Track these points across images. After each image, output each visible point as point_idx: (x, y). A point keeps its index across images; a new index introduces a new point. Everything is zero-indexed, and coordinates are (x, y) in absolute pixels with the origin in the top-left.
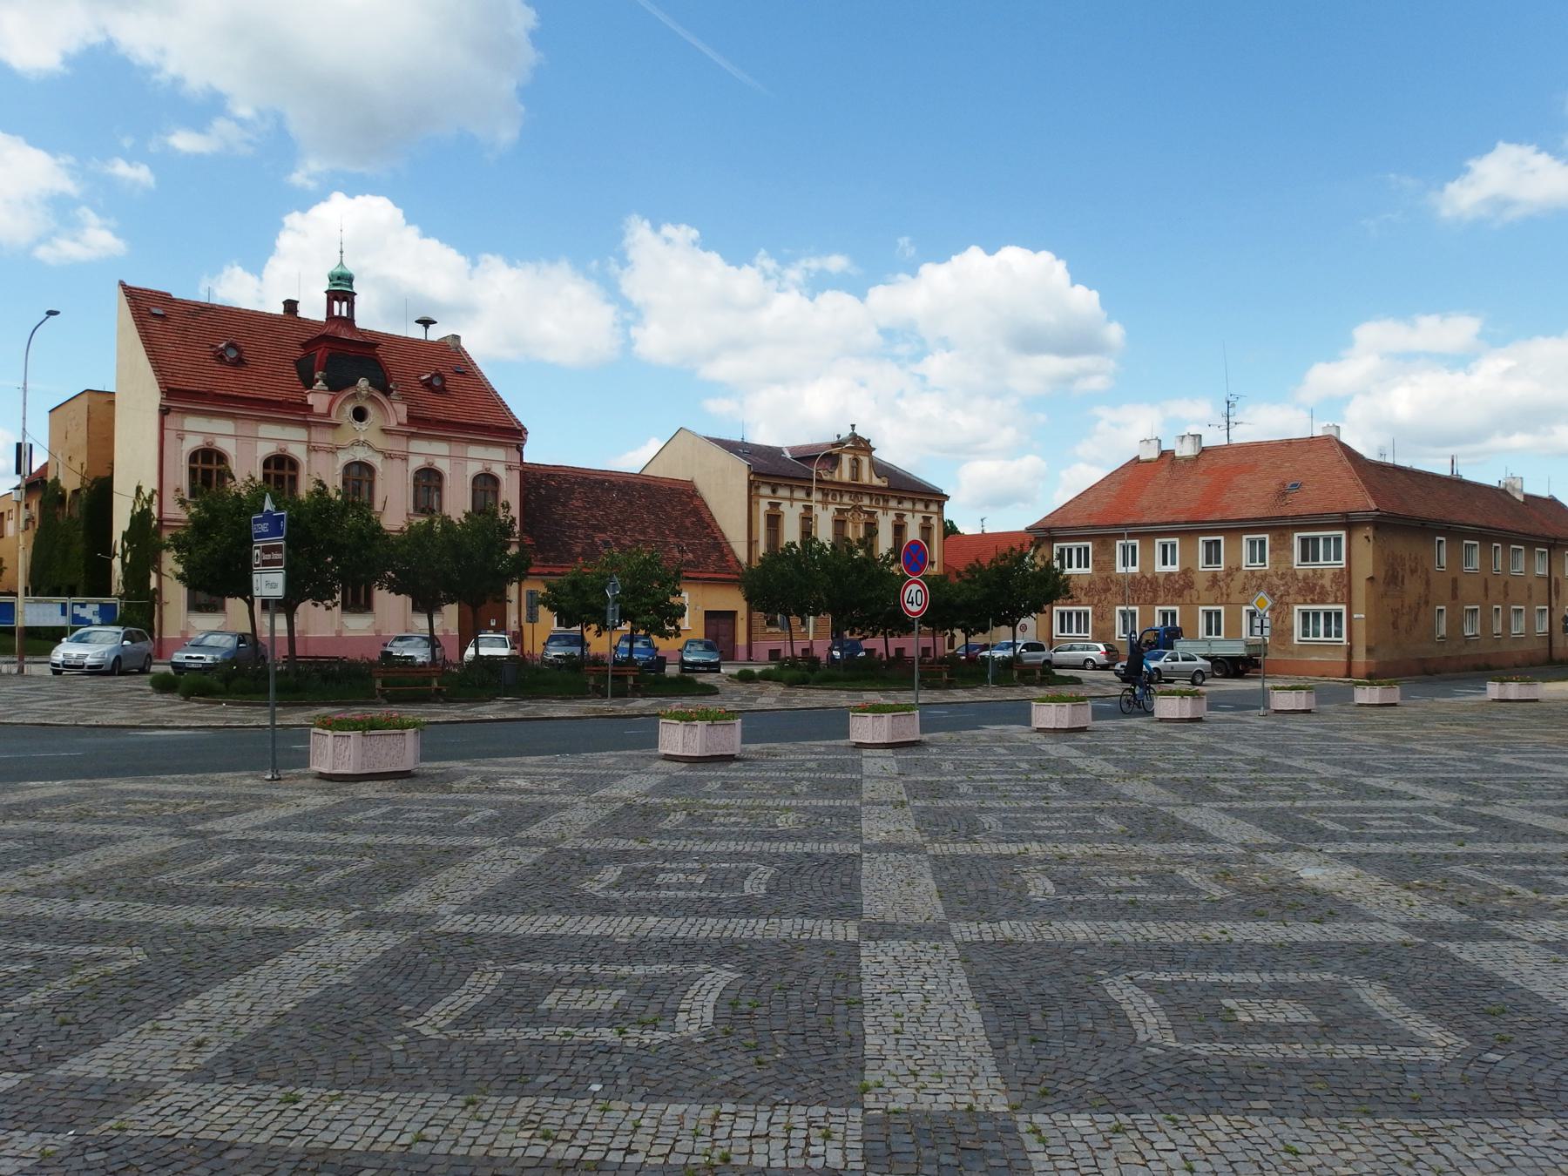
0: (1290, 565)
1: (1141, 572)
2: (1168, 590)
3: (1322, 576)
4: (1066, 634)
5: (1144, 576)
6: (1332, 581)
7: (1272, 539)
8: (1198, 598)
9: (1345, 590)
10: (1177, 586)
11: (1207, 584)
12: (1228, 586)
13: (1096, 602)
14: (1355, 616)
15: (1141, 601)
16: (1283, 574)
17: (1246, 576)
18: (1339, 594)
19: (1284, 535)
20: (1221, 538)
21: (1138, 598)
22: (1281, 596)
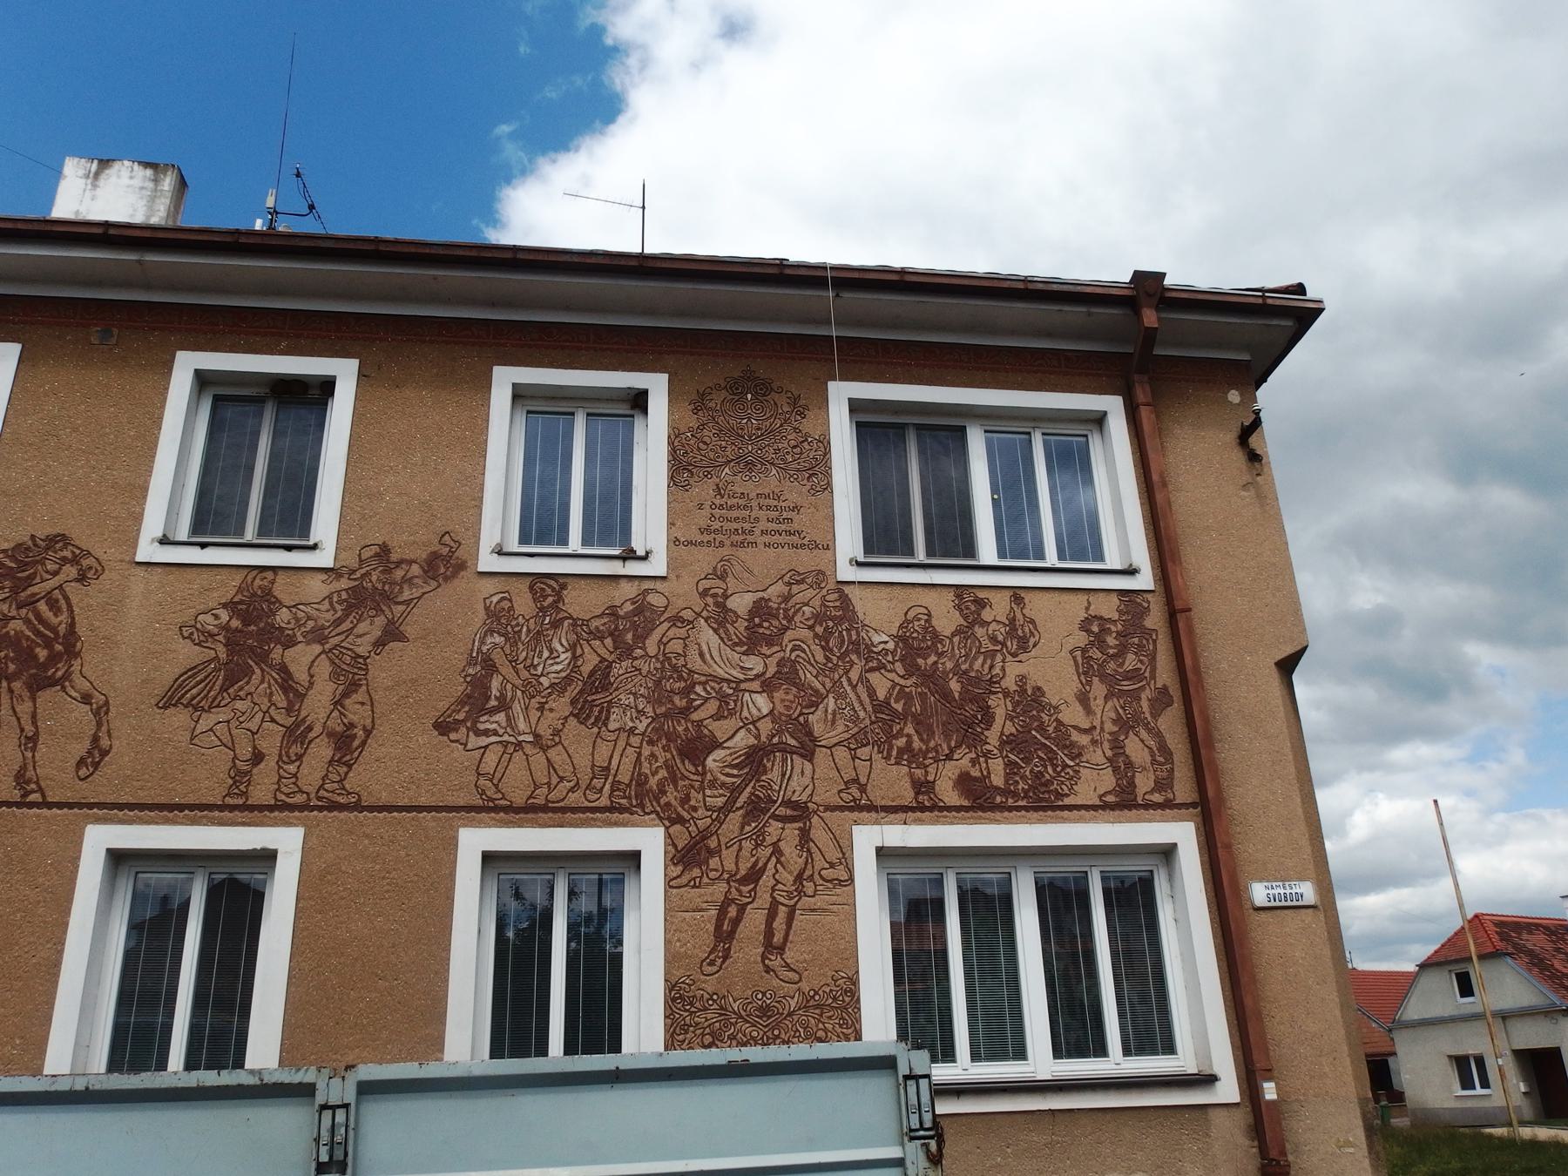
0: (806, 561)
3: (1020, 637)
6: (1087, 668)
8: (95, 756)
9: (1170, 723)
11: (188, 654)
12: (351, 677)
14: (1260, 893)
16: (760, 609)
17: (498, 617)
18: (1136, 749)
19: (763, 389)
20: (345, 372)
22: (755, 759)
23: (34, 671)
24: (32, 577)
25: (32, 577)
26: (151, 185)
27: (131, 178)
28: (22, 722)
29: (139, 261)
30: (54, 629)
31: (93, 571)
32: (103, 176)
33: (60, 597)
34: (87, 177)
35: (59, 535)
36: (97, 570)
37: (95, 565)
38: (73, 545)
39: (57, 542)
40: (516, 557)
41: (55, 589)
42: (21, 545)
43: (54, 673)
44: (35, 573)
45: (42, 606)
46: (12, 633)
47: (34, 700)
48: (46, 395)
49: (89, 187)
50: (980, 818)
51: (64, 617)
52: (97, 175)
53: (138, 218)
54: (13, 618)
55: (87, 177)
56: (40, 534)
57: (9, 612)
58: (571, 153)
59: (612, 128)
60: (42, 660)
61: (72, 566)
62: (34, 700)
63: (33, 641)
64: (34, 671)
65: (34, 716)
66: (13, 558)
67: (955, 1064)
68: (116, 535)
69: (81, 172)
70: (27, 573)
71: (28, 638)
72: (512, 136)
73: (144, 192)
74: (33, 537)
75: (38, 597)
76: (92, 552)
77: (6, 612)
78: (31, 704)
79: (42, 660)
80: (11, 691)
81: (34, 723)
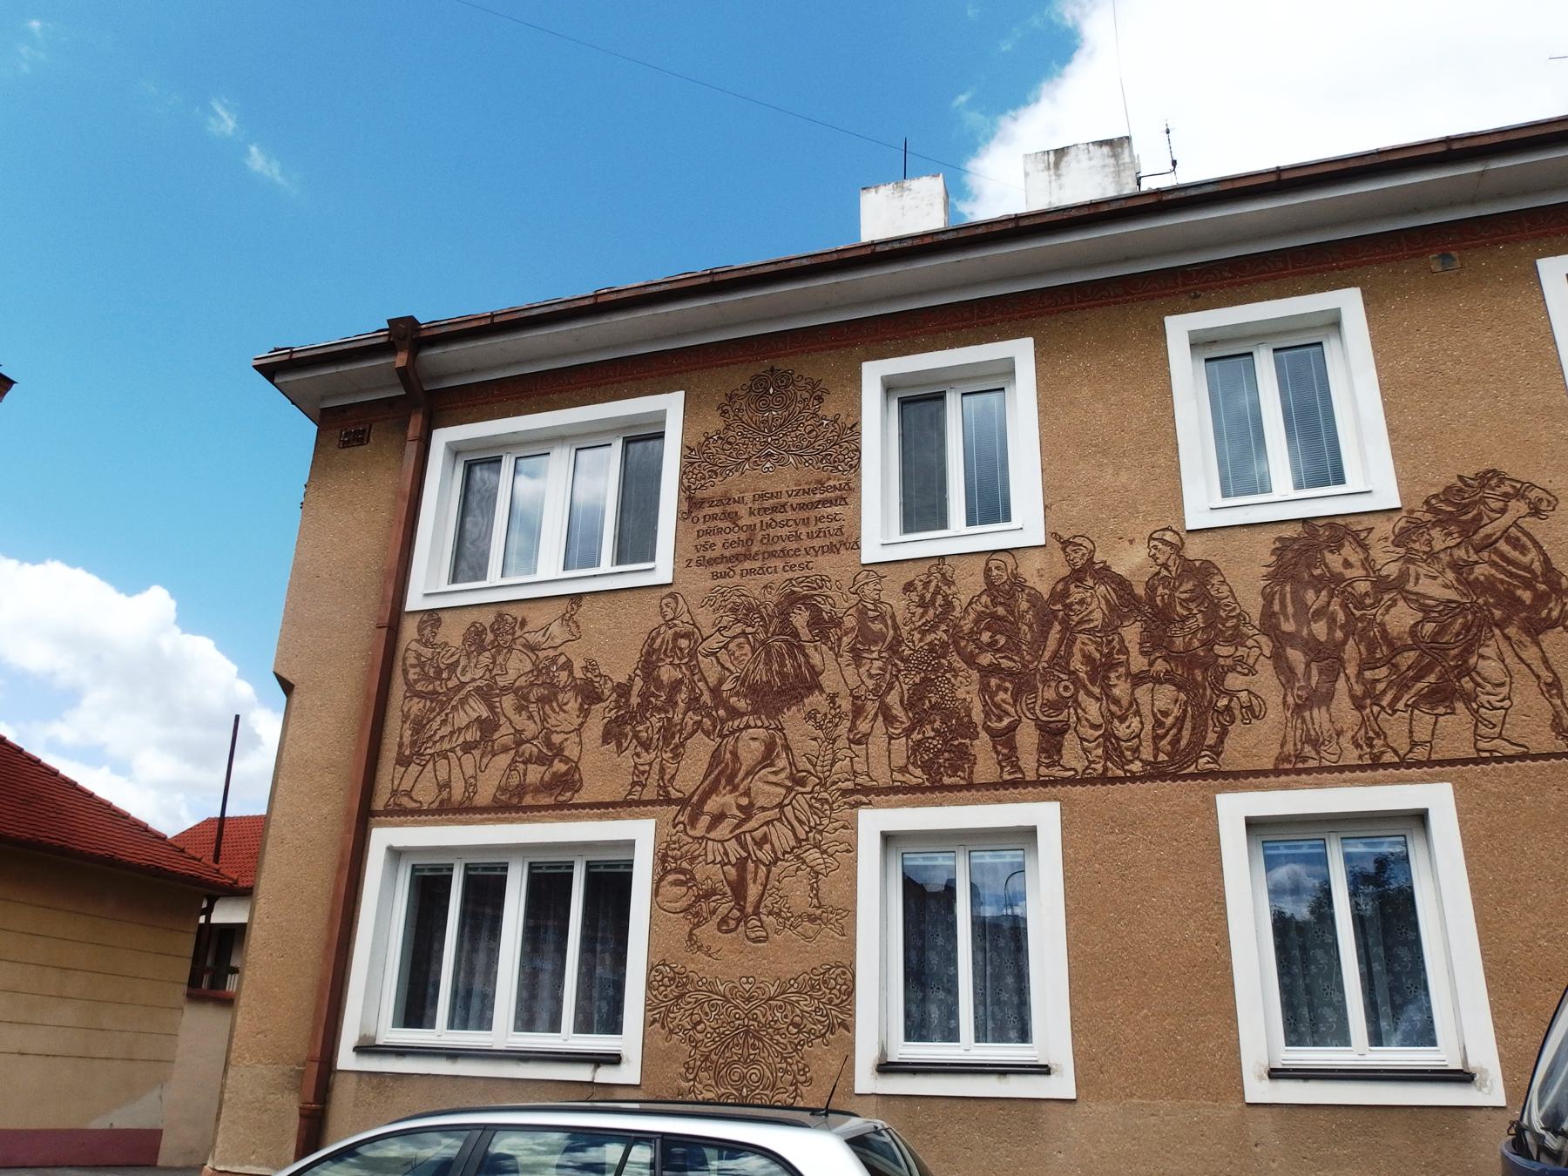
1: (1061, 541)
2: (1327, 657)
4: (440, 1034)
5: (1086, 571)
7: (1042, 355)
10: (1400, 618)
13: (691, 772)
15: (1072, 757)
21: (1052, 738)
23: (1524, 614)
24: (1478, 518)
25: (1479, 517)
26: (1112, 161)
27: (1090, 159)
28: (1535, 669)
29: (1482, 174)
30: (1528, 569)
31: (1545, 503)
32: (1063, 164)
33: (1519, 534)
34: (1048, 168)
35: (1489, 471)
36: (1549, 501)
37: (1544, 495)
38: (1509, 479)
39: (1489, 479)
40: (520, 588)
41: (1510, 526)
42: (1449, 487)
43: (1549, 613)
44: (1480, 514)
45: (1503, 546)
46: (1482, 578)
47: (1539, 645)
48: (1408, 333)
49: (1053, 177)
50: (573, 815)
51: (1533, 553)
52: (1057, 165)
53: (1111, 192)
54: (1476, 563)
55: (1048, 168)
56: (1469, 473)
57: (1469, 557)
58: (1032, 106)
59: (1070, 69)
60: (1528, 602)
61: (1518, 500)
62: (1539, 645)
63: (1509, 584)
64: (1524, 614)
65: (1545, 661)
66: (1447, 502)
67: (1348, 1048)
68: (1555, 462)
69: (1042, 166)
70: (1471, 515)
71: (1502, 582)
72: (971, 104)
73: (1107, 170)
74: (1460, 477)
75: (1494, 537)
76: (1533, 481)
77: (1466, 558)
78: (1536, 649)
79: (1528, 602)
80: (1507, 638)
81: (1549, 668)
